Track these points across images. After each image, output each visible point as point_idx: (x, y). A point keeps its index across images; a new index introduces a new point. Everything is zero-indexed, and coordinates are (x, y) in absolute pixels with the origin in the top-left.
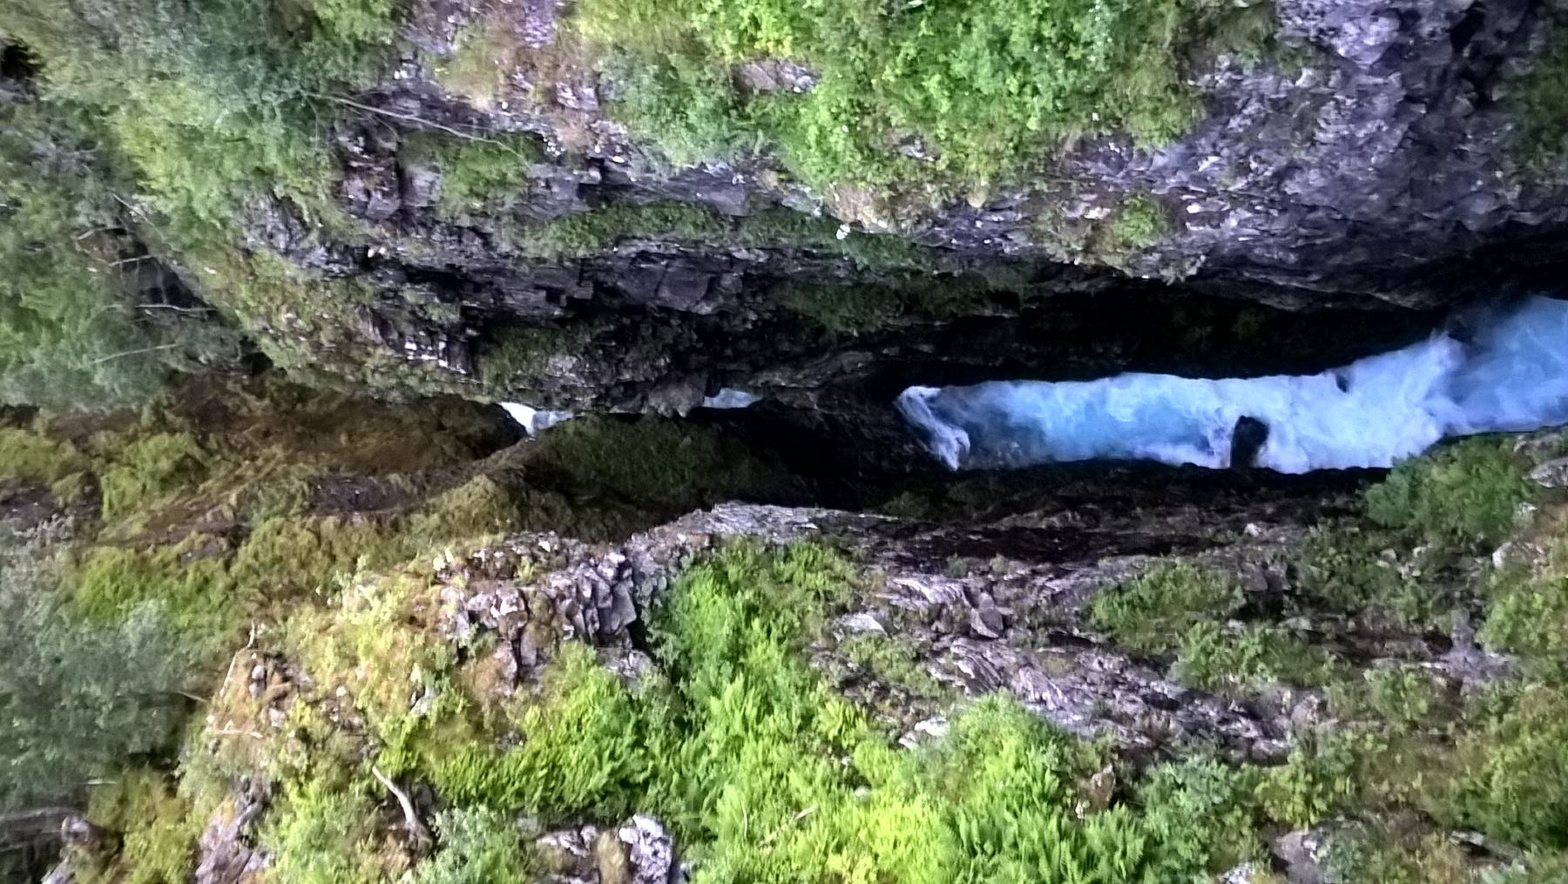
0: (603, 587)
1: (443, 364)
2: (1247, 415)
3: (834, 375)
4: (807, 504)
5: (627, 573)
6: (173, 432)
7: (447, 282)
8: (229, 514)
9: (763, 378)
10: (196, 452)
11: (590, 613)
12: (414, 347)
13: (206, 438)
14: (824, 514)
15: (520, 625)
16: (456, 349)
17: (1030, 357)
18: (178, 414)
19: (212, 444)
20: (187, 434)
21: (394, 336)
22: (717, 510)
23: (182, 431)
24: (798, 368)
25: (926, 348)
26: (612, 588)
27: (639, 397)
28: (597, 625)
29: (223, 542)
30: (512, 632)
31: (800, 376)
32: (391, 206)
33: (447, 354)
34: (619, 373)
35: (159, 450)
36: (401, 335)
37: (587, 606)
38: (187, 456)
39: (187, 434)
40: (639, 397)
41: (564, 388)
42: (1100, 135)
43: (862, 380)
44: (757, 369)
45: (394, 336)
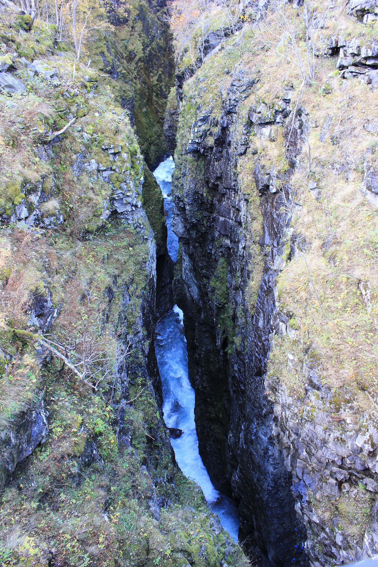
0: (129, 200)
1: (190, 141)
2: (183, 435)
3: (187, 285)
4: (157, 274)
5: (134, 208)
6: (143, 50)
7: (222, 141)
8: (119, 70)
9: (186, 258)
10: (137, 58)
11: (121, 195)
12: (196, 131)
13: (142, 61)
14: (155, 280)
15: (117, 170)
16: (195, 146)
17: (200, 355)
18: (150, 51)
19: (140, 64)
20: (143, 55)
21: (200, 124)
22: (154, 241)
23: (144, 53)
24: (190, 270)
25: (202, 316)
26: (129, 203)
27: (179, 213)
28: (117, 198)
29: (109, 68)
30: (114, 168)
31: (187, 272)
32: (254, 119)
33: (193, 143)
34: (189, 204)
35: (137, 46)
36: (200, 126)
37: (123, 194)
38: (136, 55)
39: (143, 55)
40: (179, 213)
41: (182, 185)
42: (135, 348)
43: (186, 294)
44: (191, 256)
45: (200, 124)
